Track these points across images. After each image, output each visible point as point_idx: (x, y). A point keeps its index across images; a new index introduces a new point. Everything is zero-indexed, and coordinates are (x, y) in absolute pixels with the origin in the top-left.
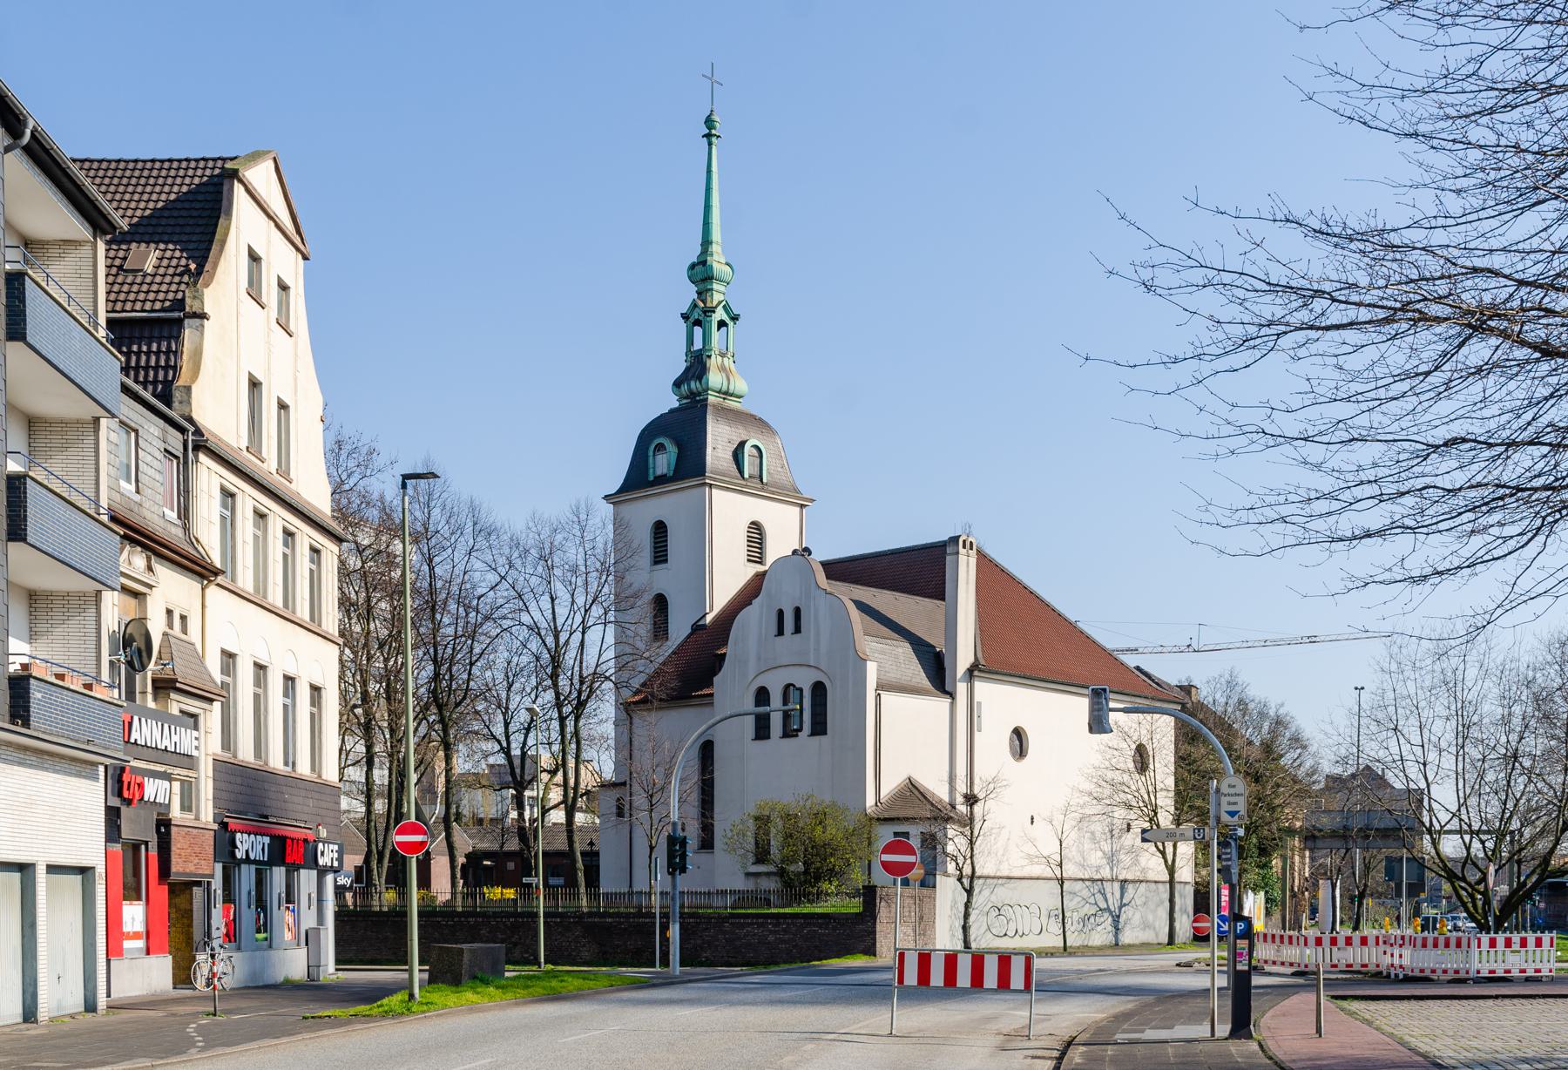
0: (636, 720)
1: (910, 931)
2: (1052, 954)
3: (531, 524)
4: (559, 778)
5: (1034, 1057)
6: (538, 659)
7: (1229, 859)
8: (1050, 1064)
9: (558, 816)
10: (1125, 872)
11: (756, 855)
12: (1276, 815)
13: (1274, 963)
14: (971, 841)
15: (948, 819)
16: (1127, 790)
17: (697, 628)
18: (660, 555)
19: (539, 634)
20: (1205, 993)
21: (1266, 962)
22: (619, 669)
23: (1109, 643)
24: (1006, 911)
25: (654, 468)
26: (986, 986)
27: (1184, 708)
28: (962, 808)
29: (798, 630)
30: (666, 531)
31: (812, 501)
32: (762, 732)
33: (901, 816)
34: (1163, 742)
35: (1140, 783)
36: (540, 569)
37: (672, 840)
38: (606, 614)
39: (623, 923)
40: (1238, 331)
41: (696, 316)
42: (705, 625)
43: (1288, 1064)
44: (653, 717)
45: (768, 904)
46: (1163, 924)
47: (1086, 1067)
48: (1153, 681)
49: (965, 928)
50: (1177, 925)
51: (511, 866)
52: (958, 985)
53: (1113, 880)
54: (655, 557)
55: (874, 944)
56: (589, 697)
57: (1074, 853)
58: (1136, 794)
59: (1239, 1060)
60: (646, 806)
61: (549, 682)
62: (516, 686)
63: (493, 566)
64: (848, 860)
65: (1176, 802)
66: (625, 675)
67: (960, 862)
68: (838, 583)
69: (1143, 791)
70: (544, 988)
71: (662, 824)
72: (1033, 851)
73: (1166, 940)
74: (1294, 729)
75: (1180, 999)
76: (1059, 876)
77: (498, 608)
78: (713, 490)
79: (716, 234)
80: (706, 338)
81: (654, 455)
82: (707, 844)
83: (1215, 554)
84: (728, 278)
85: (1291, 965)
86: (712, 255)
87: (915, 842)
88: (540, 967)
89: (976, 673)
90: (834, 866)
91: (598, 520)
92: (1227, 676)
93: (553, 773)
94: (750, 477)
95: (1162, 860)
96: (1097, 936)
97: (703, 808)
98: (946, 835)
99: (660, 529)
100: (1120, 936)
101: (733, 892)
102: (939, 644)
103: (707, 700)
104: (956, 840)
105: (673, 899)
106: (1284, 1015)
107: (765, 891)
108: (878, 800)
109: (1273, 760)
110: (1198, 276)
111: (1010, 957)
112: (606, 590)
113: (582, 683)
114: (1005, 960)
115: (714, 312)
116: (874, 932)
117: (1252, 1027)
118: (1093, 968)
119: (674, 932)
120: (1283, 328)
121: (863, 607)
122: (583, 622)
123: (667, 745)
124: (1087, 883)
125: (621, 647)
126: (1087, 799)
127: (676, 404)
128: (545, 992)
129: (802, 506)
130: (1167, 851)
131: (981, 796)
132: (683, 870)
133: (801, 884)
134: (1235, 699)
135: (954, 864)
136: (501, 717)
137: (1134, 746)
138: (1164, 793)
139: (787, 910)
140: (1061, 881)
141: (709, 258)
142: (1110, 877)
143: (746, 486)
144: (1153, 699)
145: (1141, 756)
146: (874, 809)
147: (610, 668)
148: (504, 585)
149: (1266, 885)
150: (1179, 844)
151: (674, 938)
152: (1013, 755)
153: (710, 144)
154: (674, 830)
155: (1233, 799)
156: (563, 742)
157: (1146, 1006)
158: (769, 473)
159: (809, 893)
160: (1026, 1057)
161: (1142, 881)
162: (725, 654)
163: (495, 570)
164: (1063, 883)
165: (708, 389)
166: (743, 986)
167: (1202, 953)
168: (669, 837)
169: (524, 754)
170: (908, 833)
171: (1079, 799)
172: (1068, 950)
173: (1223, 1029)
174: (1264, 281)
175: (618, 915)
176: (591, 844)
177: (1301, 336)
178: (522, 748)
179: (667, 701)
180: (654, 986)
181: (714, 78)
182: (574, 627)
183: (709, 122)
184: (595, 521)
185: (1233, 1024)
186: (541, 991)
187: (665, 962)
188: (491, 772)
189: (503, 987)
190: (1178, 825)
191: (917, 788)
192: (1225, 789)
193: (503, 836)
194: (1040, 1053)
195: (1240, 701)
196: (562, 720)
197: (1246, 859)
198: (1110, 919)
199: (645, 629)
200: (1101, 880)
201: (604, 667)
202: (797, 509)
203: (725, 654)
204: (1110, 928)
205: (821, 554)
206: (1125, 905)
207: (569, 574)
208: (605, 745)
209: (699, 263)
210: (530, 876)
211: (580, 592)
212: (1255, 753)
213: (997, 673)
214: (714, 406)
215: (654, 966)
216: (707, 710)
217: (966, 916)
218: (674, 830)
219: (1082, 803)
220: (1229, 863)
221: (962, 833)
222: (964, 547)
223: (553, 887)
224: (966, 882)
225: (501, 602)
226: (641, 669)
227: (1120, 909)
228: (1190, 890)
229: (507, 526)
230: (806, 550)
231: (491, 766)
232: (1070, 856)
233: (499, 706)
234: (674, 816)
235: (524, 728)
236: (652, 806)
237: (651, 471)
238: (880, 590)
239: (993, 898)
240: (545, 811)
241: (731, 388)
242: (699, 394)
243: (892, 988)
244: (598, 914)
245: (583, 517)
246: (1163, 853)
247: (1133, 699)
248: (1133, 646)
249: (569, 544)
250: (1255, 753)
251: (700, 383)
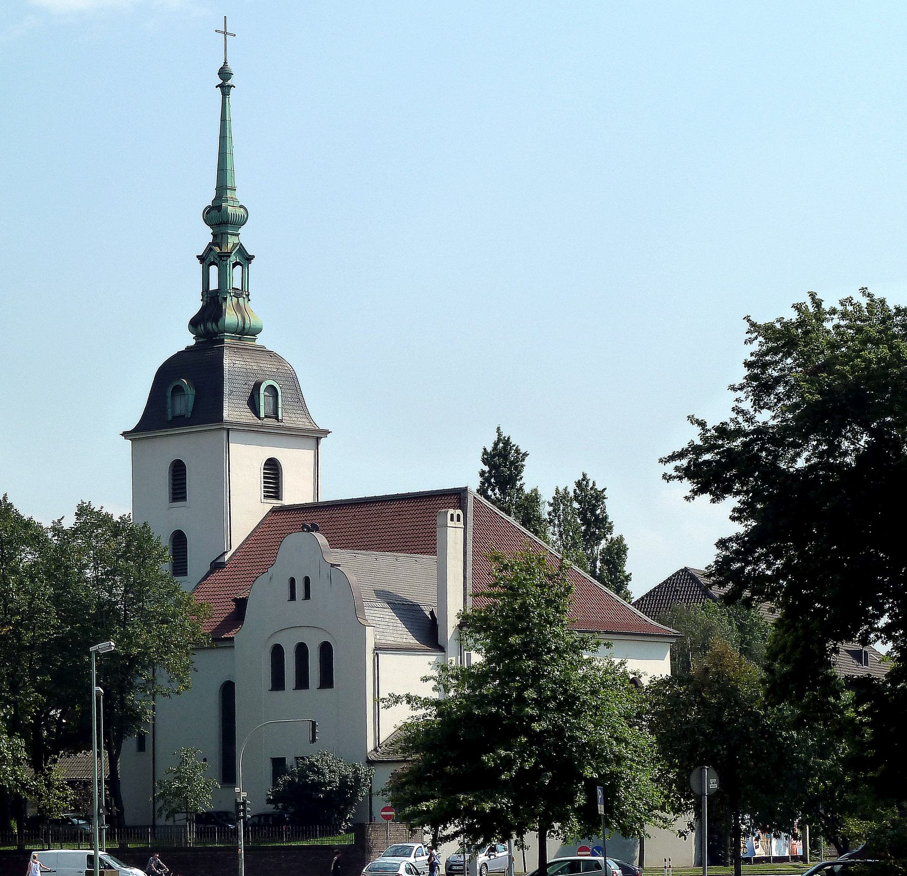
18: (178, 491)
29: (307, 596)
81: (173, 396)
94: (266, 417)
141: (223, 204)
183: (224, 74)
241: (247, 326)
242: (216, 334)
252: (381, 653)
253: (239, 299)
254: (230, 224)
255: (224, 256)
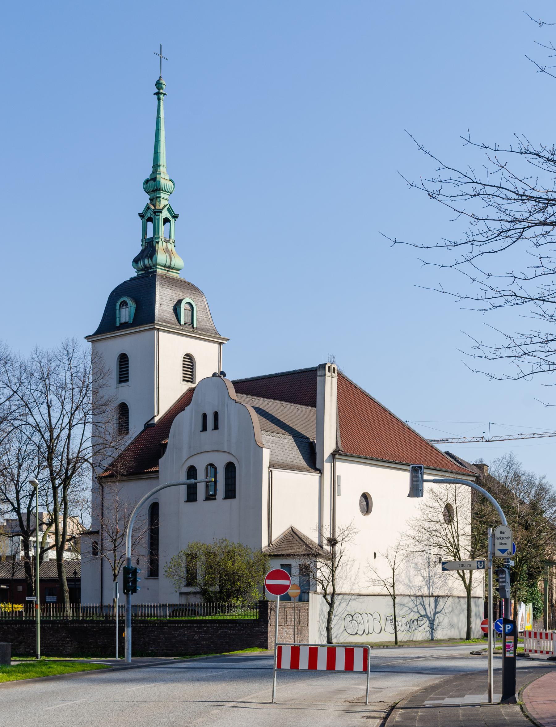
0: (106, 489)
1: (291, 631)
2: (387, 646)
3: (35, 356)
4: (53, 529)
5: (368, 717)
6: (39, 447)
7: (504, 582)
8: (379, 722)
9: (52, 554)
10: (438, 590)
11: (187, 580)
12: (540, 551)
13: (536, 651)
14: (332, 570)
15: (318, 555)
16: (438, 535)
17: (149, 426)
18: (123, 377)
19: (40, 431)
20: (485, 672)
21: (530, 651)
22: (95, 454)
23: (427, 434)
24: (358, 617)
25: (120, 318)
26: (337, 668)
27: (478, 481)
28: (327, 548)
29: (216, 427)
30: (128, 361)
31: (227, 340)
32: (192, 496)
33: (284, 553)
34: (463, 502)
35: (447, 530)
36: (41, 386)
37: (127, 571)
38: (85, 416)
39: (94, 628)
40: (497, 226)
41: (148, 215)
42: (154, 424)
43: (539, 721)
44: (116, 486)
45: (194, 613)
46: (463, 626)
47: (402, 724)
48: (457, 461)
49: (328, 629)
50: (473, 626)
51: (20, 588)
52: (300, 669)
53: (429, 596)
54: (120, 378)
55: (266, 640)
56: (73, 473)
57: (403, 578)
58: (445, 538)
59: (506, 718)
60: (111, 547)
61: (45, 464)
62: (24, 466)
63: (8, 384)
64: (249, 583)
65: (472, 543)
66: (99, 458)
67: (325, 584)
68: (244, 395)
69: (449, 536)
70: (36, 672)
71: (122, 559)
72: (375, 577)
73: (465, 636)
74: (551, 493)
75: (471, 677)
76: (392, 594)
77: (11, 412)
78: (160, 333)
79: (163, 160)
80: (156, 230)
82: (154, 572)
83: (488, 378)
84: (171, 190)
85: (547, 653)
86: (160, 174)
87: (295, 571)
88: (37, 658)
89: (337, 456)
90: (240, 587)
91: (80, 353)
92: (508, 458)
93: (49, 525)
95: (462, 582)
96: (420, 634)
97: (151, 549)
98: (315, 566)
99: (123, 359)
100: (434, 634)
101: (170, 606)
102: (312, 436)
103: (154, 475)
104: (322, 569)
105: (128, 611)
106: (539, 687)
107: (192, 605)
108: (270, 543)
109: (537, 514)
110: (469, 189)
111: (353, 649)
112: (85, 400)
113: (68, 464)
114: (350, 652)
115: (161, 212)
116: (266, 633)
117: (516, 695)
118: (414, 656)
119: (127, 633)
120: (526, 224)
121: (259, 411)
122: (70, 422)
123: (126, 506)
124: (412, 598)
125: (96, 439)
126: (412, 541)
127: (135, 275)
128: (37, 675)
129: (220, 344)
130: (466, 577)
131: (339, 539)
132: (134, 591)
133: (217, 600)
134: (511, 474)
135: (321, 586)
136: (14, 487)
137: (443, 506)
138: (464, 537)
139: (208, 618)
140: (394, 597)
141: (158, 176)
142: (427, 594)
143: (182, 330)
144: (456, 473)
145: (449, 512)
146: (267, 548)
147: (88, 453)
148: (16, 397)
149: (533, 599)
150: (474, 571)
151: (128, 637)
152: (362, 512)
153: (159, 99)
154: (129, 563)
155: (503, 541)
156: (55, 504)
157: (447, 682)
158: (198, 321)
159: (223, 606)
160: (363, 717)
161: (449, 597)
162: (167, 444)
163: (9, 387)
164: (395, 598)
165: (157, 264)
166: (174, 670)
167: (482, 646)
168: (125, 568)
169: (29, 512)
170: (290, 565)
171: (405, 541)
172: (398, 644)
173: (497, 697)
174: (514, 192)
175: (92, 621)
176: (75, 573)
177: (539, 230)
178: (28, 508)
179: (126, 476)
180: (114, 670)
181: (162, 55)
182: (64, 426)
183: (158, 85)
184: (79, 354)
185: (503, 694)
186: (34, 674)
187: (122, 654)
188: (8, 525)
189: (8, 672)
190: (473, 558)
191: (296, 534)
192: (498, 534)
193: (13, 568)
194: (372, 714)
195: (516, 475)
196: (55, 489)
197: (519, 581)
198: (428, 622)
199: (112, 427)
200: (422, 596)
201: (84, 453)
202: (217, 346)
203: (167, 444)
204: (428, 629)
205: (233, 376)
206: (438, 613)
207: (60, 390)
208: (86, 506)
209: (151, 179)
210: (31, 595)
211: (68, 400)
212: (525, 510)
213: (351, 456)
214: (161, 276)
215: (115, 657)
216: (154, 482)
217: (329, 621)
218: (129, 563)
219: (408, 544)
220: (504, 584)
221: (326, 565)
222: (329, 371)
223: (47, 603)
224: (329, 598)
225: (13, 408)
226: (109, 454)
227: (435, 615)
228: (482, 602)
229: (18, 357)
230: (223, 373)
231: (7, 520)
232: (400, 579)
233: (12, 480)
234: (128, 554)
235: (30, 494)
236: (115, 547)
237: (118, 319)
238: (272, 400)
239: (348, 608)
240: (43, 551)
242: (151, 268)
243: (273, 670)
244: (78, 621)
245: (71, 351)
246: (463, 578)
247: (443, 473)
248: (445, 437)
249: (61, 369)
250: (525, 510)
251: (152, 260)
252: (274, 470)
253: (168, 244)
254: (162, 191)
255: (157, 212)
